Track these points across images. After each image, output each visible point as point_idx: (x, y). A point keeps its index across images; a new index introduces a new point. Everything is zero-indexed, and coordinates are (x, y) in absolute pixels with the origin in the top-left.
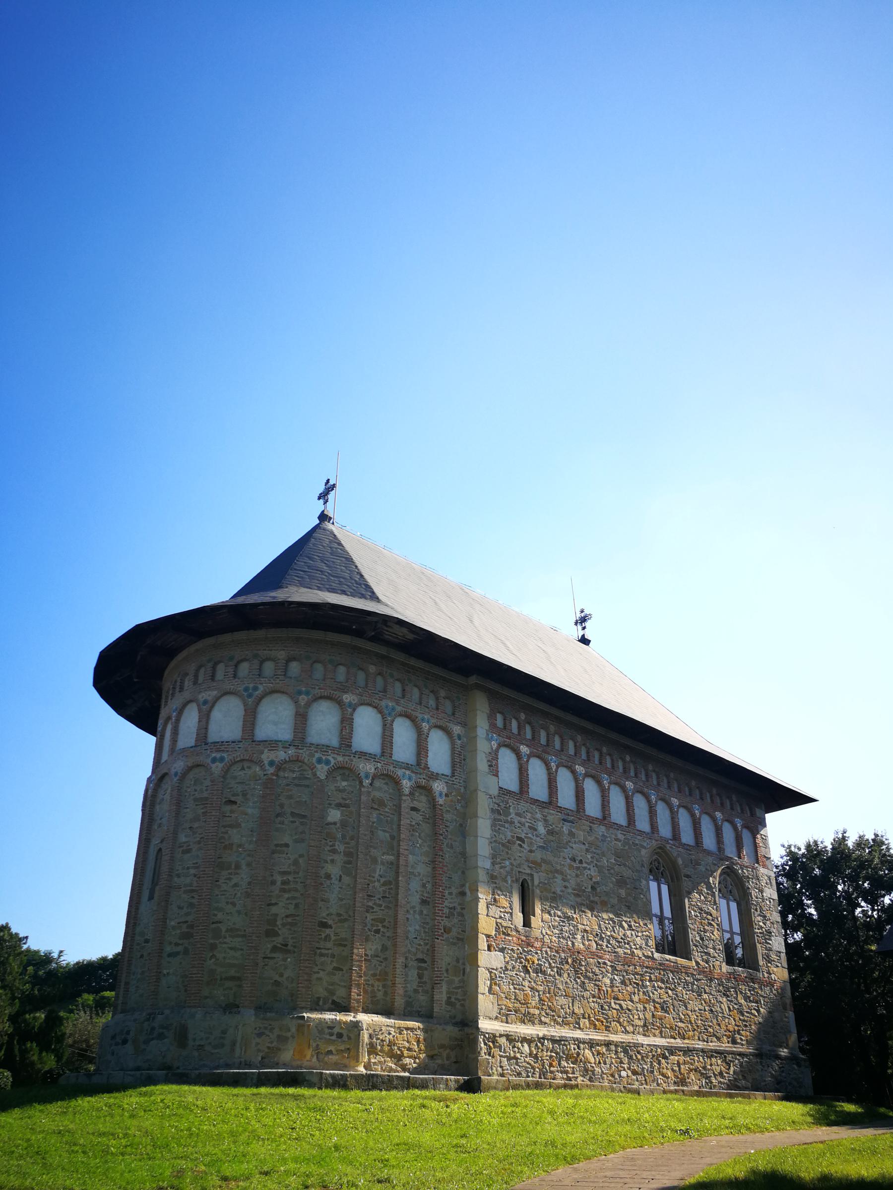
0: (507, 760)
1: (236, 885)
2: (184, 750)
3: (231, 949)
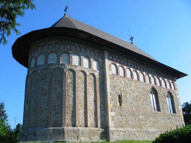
0: (113, 67)
1: (46, 99)
2: (32, 68)
3: (46, 113)
